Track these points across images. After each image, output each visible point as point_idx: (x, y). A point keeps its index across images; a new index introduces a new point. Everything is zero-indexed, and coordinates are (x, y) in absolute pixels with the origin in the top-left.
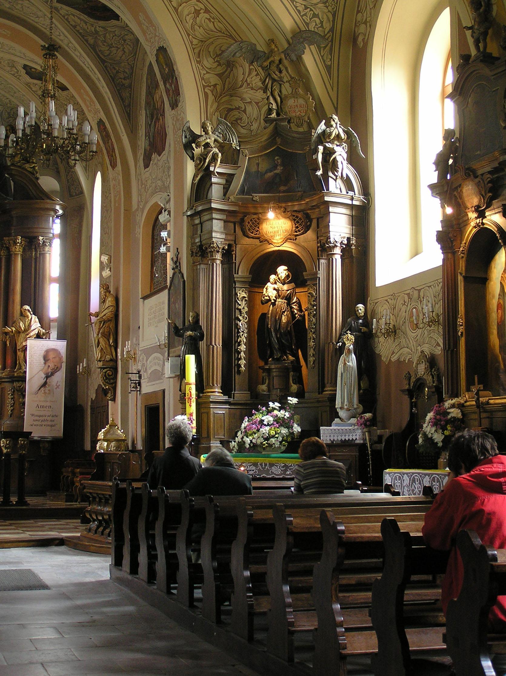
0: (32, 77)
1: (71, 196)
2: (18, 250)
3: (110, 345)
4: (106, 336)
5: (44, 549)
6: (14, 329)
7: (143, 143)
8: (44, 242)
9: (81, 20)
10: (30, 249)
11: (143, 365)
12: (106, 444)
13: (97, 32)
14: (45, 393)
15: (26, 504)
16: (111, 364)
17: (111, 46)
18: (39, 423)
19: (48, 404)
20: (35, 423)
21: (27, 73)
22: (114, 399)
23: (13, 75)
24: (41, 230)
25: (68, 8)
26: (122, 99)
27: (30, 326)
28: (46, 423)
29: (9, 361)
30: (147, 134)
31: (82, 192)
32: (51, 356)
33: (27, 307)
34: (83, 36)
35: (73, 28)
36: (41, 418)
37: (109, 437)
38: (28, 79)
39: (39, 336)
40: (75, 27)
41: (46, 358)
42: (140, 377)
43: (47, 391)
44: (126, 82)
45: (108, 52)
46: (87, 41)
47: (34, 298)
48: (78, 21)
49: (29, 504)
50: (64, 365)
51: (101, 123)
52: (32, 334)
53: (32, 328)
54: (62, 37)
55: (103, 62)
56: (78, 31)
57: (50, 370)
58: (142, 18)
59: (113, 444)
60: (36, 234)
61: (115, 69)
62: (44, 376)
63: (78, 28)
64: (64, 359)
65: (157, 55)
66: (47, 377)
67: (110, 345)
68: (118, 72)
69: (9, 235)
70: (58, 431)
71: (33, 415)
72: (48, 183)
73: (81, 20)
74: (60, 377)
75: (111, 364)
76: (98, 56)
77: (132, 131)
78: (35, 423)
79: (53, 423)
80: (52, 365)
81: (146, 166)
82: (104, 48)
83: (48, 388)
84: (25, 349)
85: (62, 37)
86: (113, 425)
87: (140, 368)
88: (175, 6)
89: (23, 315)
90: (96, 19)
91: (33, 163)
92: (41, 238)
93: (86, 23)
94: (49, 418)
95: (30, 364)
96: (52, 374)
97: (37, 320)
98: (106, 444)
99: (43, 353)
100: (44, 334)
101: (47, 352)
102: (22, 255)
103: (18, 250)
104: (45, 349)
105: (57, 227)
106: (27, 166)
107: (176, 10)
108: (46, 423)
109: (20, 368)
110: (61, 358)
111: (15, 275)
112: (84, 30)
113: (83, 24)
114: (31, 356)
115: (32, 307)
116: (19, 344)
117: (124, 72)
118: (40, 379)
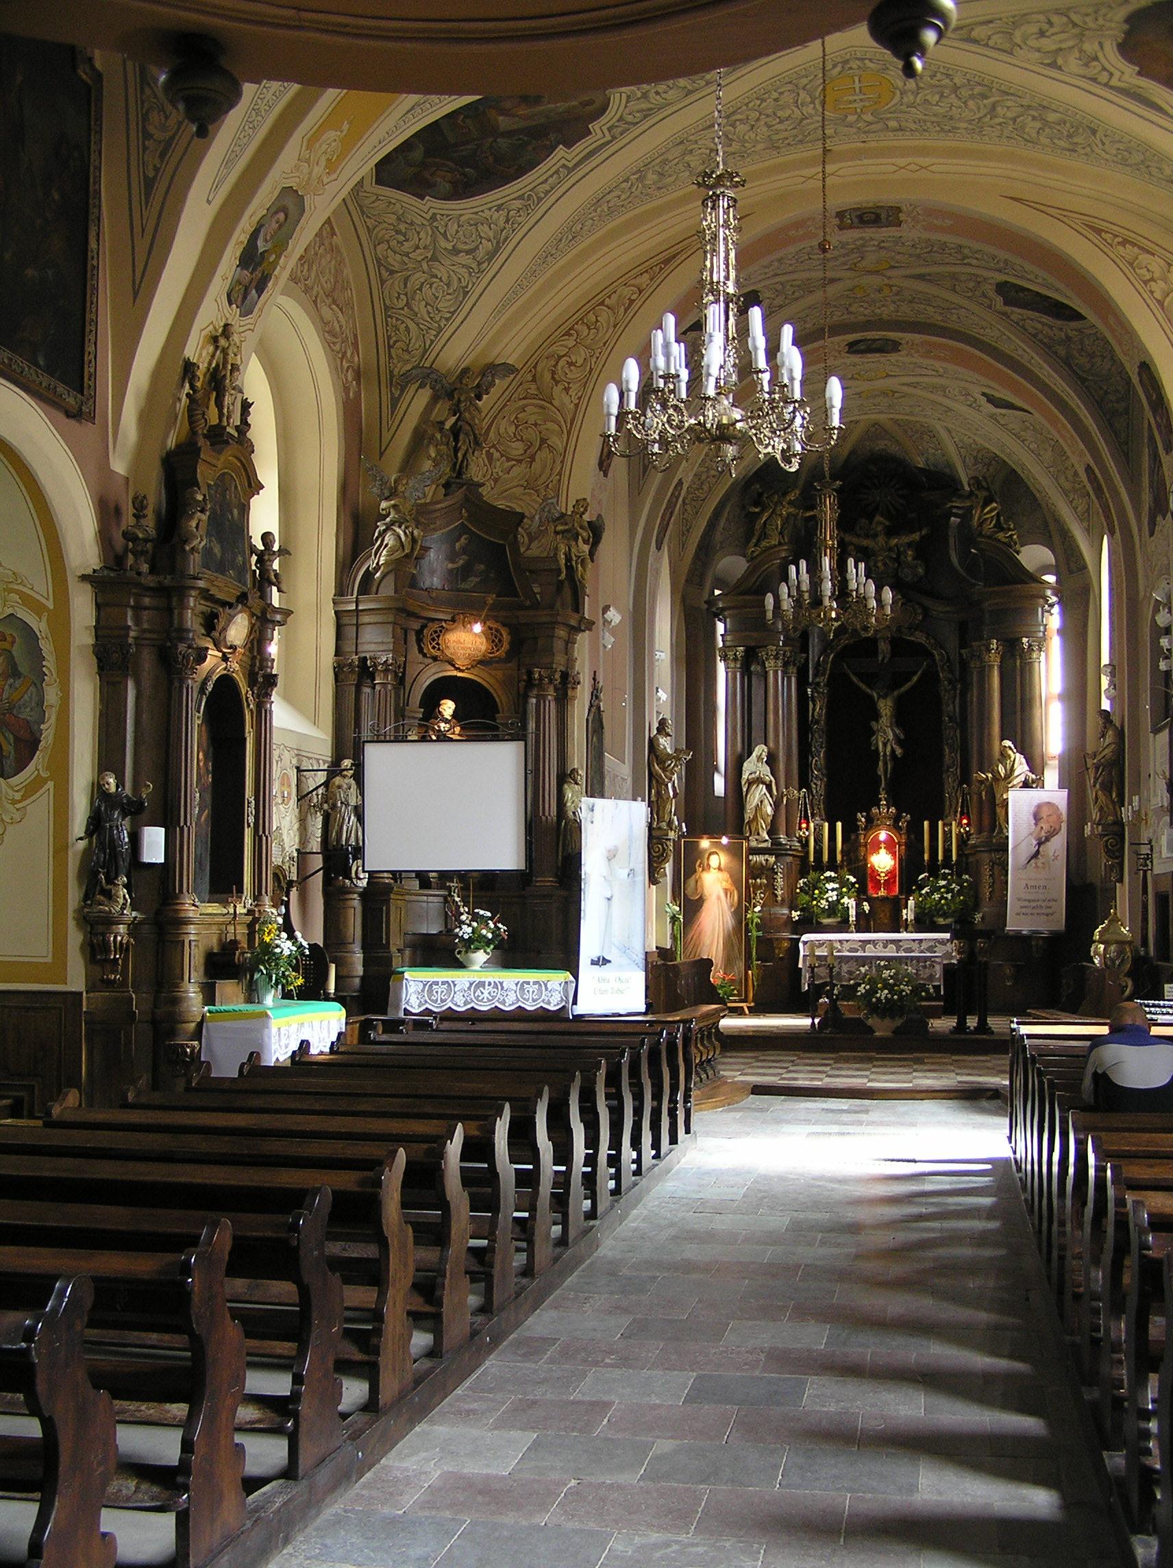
0: (997, 407)
1: (1071, 572)
2: (994, 659)
3: (1113, 802)
4: (1106, 788)
5: (967, 1103)
6: (990, 775)
7: (1147, 498)
8: (1030, 645)
9: (1043, 324)
10: (1013, 656)
11: (1155, 832)
12: (1102, 947)
13: (1069, 339)
14: (1037, 867)
15: (989, 1031)
16: (1116, 828)
17: (1092, 356)
18: (1029, 911)
19: (1042, 883)
20: (1024, 910)
21: (989, 401)
22: (1121, 880)
23: (970, 406)
24: (1025, 629)
25: (1019, 311)
26: (1116, 434)
27: (1012, 770)
28: (1039, 911)
29: (986, 822)
30: (1151, 486)
31: (1085, 567)
32: (1044, 813)
33: (1007, 743)
34: (1050, 348)
35: (1033, 338)
36: (1033, 904)
37: (1106, 937)
38: (991, 408)
39: (1026, 785)
40: (1035, 336)
41: (1037, 817)
42: (1152, 850)
43: (1040, 865)
44: (1121, 406)
45: (1088, 366)
46: (1056, 353)
47: (1020, 726)
48: (1039, 326)
49: (993, 1033)
50: (1064, 826)
51: (1088, 469)
52: (1015, 782)
53: (1016, 773)
54: (1020, 352)
55: (1083, 380)
56: (1041, 341)
57: (1043, 834)
58: (1112, 321)
59: (1113, 948)
60: (1018, 635)
61: (1101, 388)
62: (1035, 842)
63: (1040, 336)
64: (1064, 817)
65: (1139, 374)
66: (1040, 844)
67: (1113, 802)
68: (1106, 393)
69: (981, 638)
70: (1057, 921)
71: (1019, 900)
72: (1034, 556)
73: (1043, 324)
74: (1058, 845)
75: (1116, 828)
76: (1075, 372)
77: (1132, 480)
78: (1024, 910)
79: (1050, 911)
80: (1046, 827)
81: (1152, 534)
82: (1083, 360)
83: (1041, 859)
84: (1005, 804)
85: (1020, 352)
86: (1115, 920)
87: (1151, 835)
88: (1159, 297)
89: (1004, 756)
90: (1065, 319)
91: (1010, 530)
92: (1025, 640)
93: (1051, 327)
94: (1044, 904)
95: (1014, 825)
96: (1047, 839)
97: (1024, 761)
98: (1102, 947)
99: (1032, 809)
100: (1033, 782)
101: (1039, 807)
102: (1001, 667)
103: (994, 659)
104: (1035, 803)
105: (1054, 620)
106: (1001, 535)
107: (1161, 303)
108: (1039, 911)
109: (1001, 831)
110: (1059, 816)
111: (991, 697)
112: (1050, 338)
113: (1046, 330)
114: (1015, 815)
115: (1019, 743)
116: (998, 796)
117: (1117, 391)
118: (1030, 846)
